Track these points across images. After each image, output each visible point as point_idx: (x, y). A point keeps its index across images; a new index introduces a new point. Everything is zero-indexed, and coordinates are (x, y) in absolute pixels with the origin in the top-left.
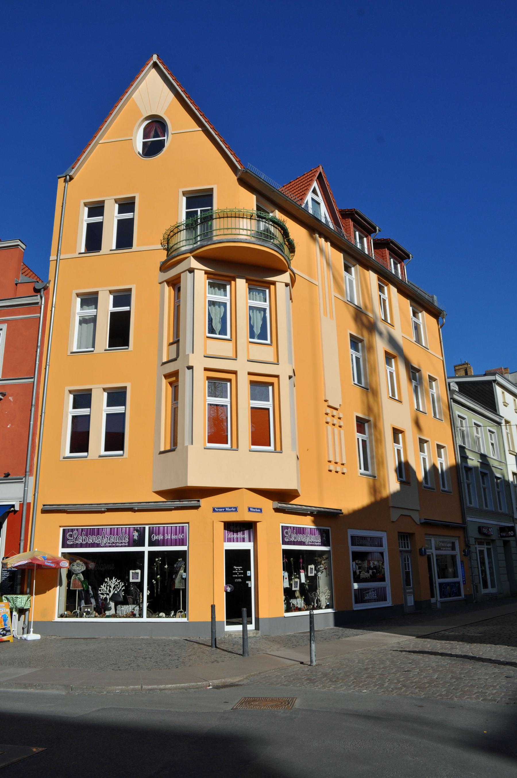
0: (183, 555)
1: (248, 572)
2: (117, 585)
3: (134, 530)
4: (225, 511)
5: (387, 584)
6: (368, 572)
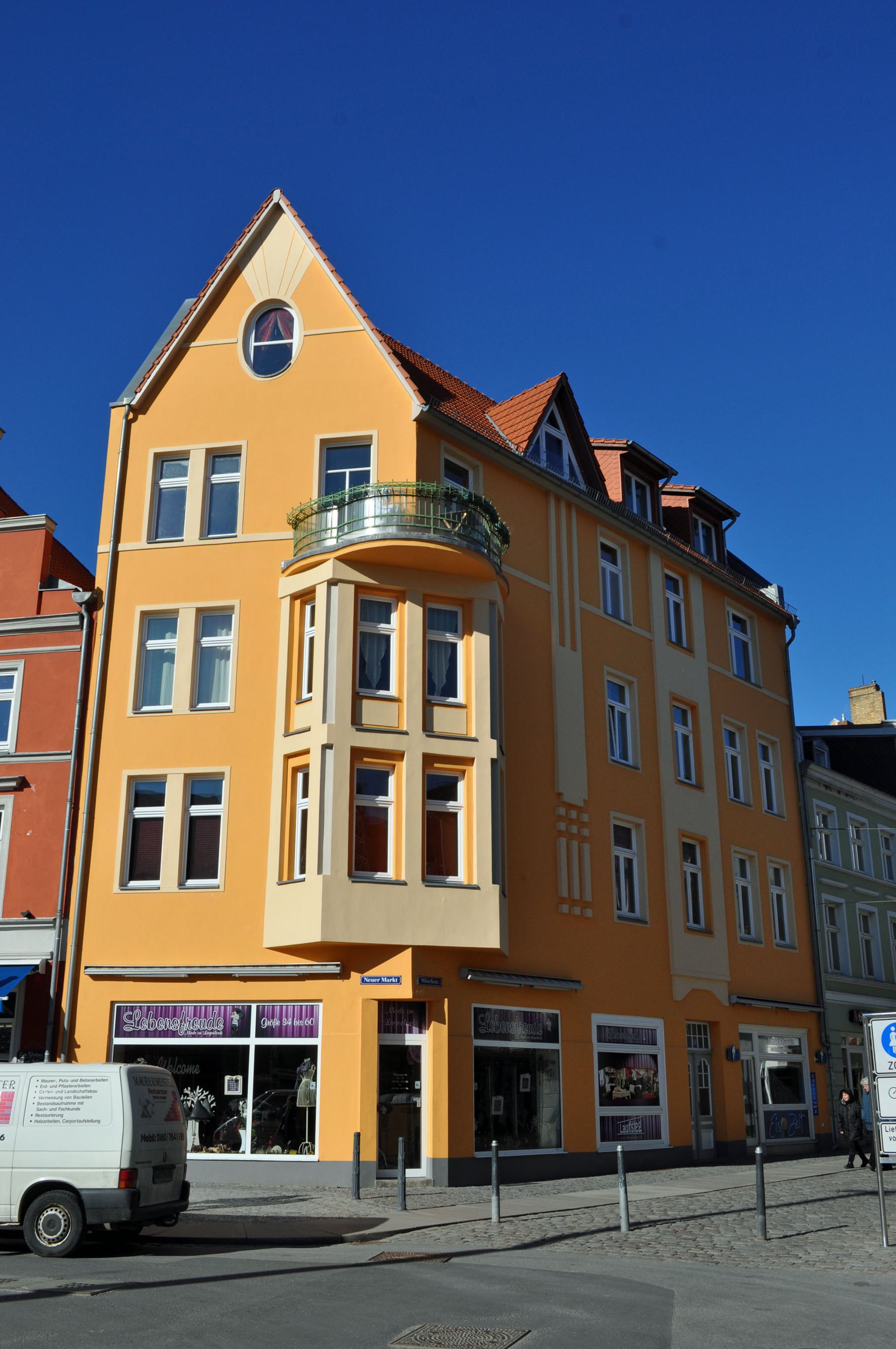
0: (311, 1052)
1: (417, 1083)
2: (203, 1100)
3: (233, 1011)
4: (380, 982)
5: (662, 1110)
6: (628, 1089)
